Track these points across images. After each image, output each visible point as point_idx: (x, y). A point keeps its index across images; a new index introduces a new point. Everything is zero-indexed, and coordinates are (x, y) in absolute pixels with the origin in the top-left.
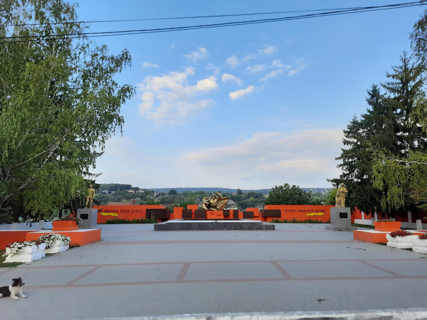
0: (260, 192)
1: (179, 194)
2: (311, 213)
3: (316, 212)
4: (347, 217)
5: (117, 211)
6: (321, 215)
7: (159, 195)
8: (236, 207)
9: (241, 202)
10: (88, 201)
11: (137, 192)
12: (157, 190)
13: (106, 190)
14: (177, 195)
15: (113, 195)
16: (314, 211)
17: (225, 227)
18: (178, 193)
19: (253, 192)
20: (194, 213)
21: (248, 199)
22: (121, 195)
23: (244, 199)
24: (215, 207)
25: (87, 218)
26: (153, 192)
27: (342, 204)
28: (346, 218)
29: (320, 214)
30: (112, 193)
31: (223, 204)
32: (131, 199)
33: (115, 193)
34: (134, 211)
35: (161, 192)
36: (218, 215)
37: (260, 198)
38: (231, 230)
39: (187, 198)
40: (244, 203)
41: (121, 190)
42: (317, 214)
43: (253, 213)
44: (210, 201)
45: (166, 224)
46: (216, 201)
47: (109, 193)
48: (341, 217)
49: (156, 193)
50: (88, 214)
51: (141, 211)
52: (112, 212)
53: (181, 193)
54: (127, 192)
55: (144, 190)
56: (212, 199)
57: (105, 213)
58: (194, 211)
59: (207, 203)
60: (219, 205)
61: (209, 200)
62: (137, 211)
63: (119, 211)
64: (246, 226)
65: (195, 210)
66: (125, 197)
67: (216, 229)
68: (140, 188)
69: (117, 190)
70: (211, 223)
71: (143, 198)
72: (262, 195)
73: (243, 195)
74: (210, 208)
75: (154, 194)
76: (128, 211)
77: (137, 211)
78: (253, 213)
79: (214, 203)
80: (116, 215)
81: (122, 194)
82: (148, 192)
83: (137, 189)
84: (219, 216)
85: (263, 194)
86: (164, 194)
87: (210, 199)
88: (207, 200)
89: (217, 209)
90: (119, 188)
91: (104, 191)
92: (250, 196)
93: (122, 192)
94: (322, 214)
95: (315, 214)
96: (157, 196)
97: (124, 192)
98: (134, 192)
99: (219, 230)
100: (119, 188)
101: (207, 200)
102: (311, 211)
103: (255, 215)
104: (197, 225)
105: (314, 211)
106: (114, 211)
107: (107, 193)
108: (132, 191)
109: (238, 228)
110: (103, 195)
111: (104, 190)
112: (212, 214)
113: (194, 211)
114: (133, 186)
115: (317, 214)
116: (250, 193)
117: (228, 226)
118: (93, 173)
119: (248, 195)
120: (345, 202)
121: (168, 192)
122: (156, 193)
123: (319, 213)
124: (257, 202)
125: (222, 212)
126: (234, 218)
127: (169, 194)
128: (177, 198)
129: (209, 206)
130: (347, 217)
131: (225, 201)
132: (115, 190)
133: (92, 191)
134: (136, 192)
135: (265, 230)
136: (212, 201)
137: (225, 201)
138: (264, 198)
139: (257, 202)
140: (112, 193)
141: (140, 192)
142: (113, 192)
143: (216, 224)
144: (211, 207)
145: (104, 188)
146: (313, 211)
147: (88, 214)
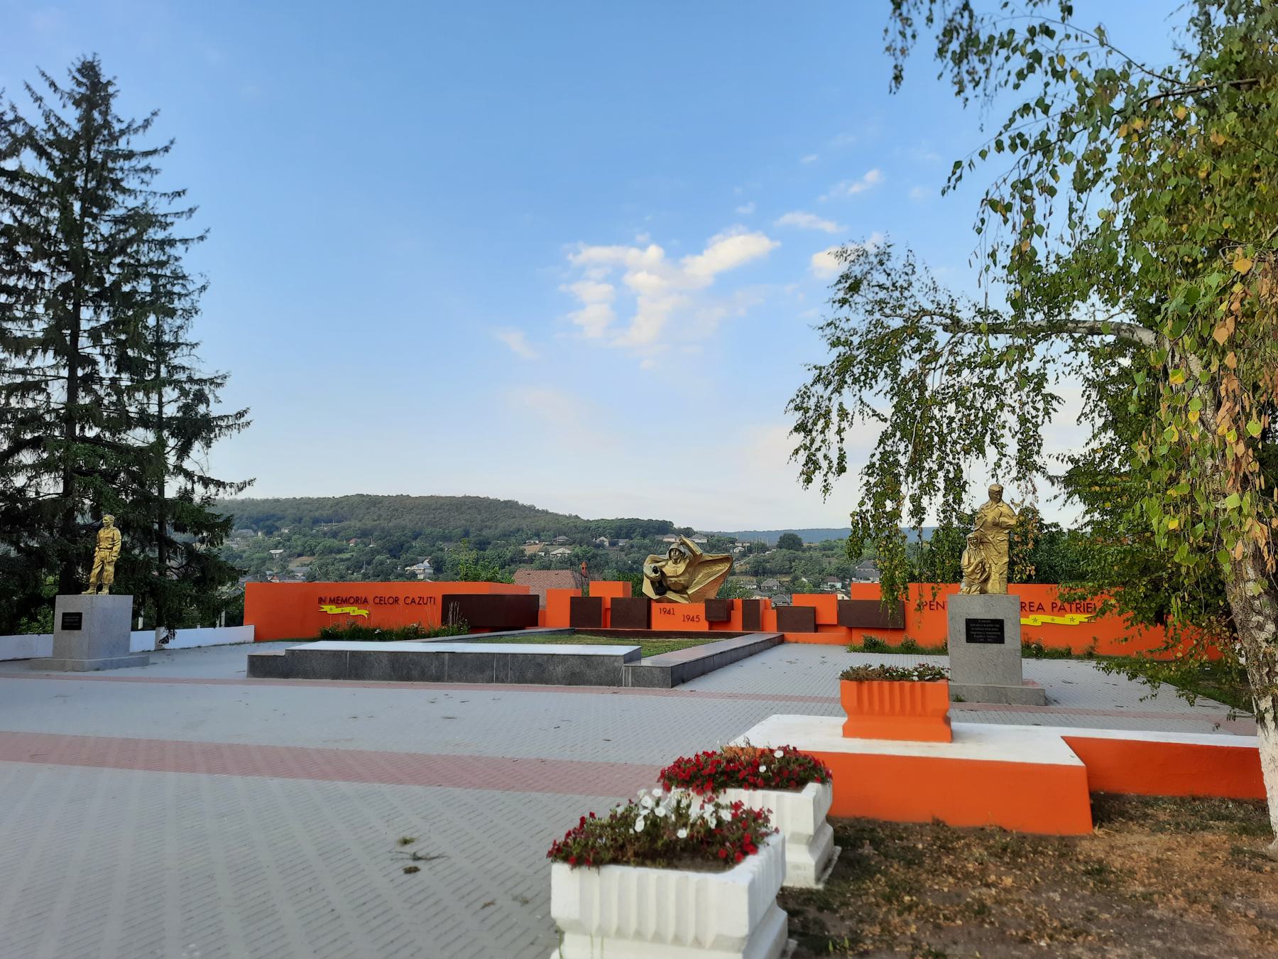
1: (810, 548)
2: (1032, 617)
3: (1055, 610)
4: (1000, 639)
5: (366, 601)
6: (1039, 623)
7: (750, 550)
10: (97, 571)
14: (804, 551)
15: (622, 549)
16: (1047, 607)
17: (483, 672)
18: (805, 545)
24: (682, 590)
25: (79, 628)
26: (733, 541)
27: (993, 577)
28: (995, 645)
29: (1072, 619)
30: (620, 544)
31: (712, 579)
34: (413, 601)
38: (503, 681)
39: (834, 560)
41: (644, 536)
42: (1058, 620)
44: (664, 570)
45: (283, 654)
46: (681, 567)
47: (613, 544)
48: (970, 638)
49: (740, 545)
50: (80, 615)
52: (352, 604)
53: (817, 544)
54: (661, 542)
55: (707, 535)
57: (333, 607)
60: (698, 583)
62: (421, 602)
63: (370, 600)
64: (560, 670)
65: (612, 599)
67: (451, 679)
69: (633, 536)
70: (434, 653)
74: (665, 593)
76: (396, 600)
77: (421, 602)
79: (677, 577)
80: (364, 612)
82: (718, 541)
83: (688, 532)
84: (693, 620)
86: (764, 548)
87: (664, 560)
89: (690, 598)
91: (598, 541)
93: (647, 541)
94: (1079, 618)
95: (1047, 618)
96: (744, 555)
97: (652, 541)
99: (460, 680)
102: (1035, 609)
104: (385, 661)
105: (1047, 607)
106: (357, 601)
107: (607, 544)
109: (529, 675)
111: (600, 536)
114: (676, 526)
115: (1058, 620)
118: (227, 481)
120: (1006, 566)
121: (776, 541)
122: (740, 545)
123: (1069, 616)
126: (743, 629)
127: (780, 547)
128: (801, 559)
129: (661, 585)
130: (1000, 639)
132: (628, 536)
133: (111, 535)
135: (633, 685)
137: (718, 568)
142: (622, 543)
143: (450, 659)
144: (670, 589)
146: (1041, 609)
147: (81, 614)
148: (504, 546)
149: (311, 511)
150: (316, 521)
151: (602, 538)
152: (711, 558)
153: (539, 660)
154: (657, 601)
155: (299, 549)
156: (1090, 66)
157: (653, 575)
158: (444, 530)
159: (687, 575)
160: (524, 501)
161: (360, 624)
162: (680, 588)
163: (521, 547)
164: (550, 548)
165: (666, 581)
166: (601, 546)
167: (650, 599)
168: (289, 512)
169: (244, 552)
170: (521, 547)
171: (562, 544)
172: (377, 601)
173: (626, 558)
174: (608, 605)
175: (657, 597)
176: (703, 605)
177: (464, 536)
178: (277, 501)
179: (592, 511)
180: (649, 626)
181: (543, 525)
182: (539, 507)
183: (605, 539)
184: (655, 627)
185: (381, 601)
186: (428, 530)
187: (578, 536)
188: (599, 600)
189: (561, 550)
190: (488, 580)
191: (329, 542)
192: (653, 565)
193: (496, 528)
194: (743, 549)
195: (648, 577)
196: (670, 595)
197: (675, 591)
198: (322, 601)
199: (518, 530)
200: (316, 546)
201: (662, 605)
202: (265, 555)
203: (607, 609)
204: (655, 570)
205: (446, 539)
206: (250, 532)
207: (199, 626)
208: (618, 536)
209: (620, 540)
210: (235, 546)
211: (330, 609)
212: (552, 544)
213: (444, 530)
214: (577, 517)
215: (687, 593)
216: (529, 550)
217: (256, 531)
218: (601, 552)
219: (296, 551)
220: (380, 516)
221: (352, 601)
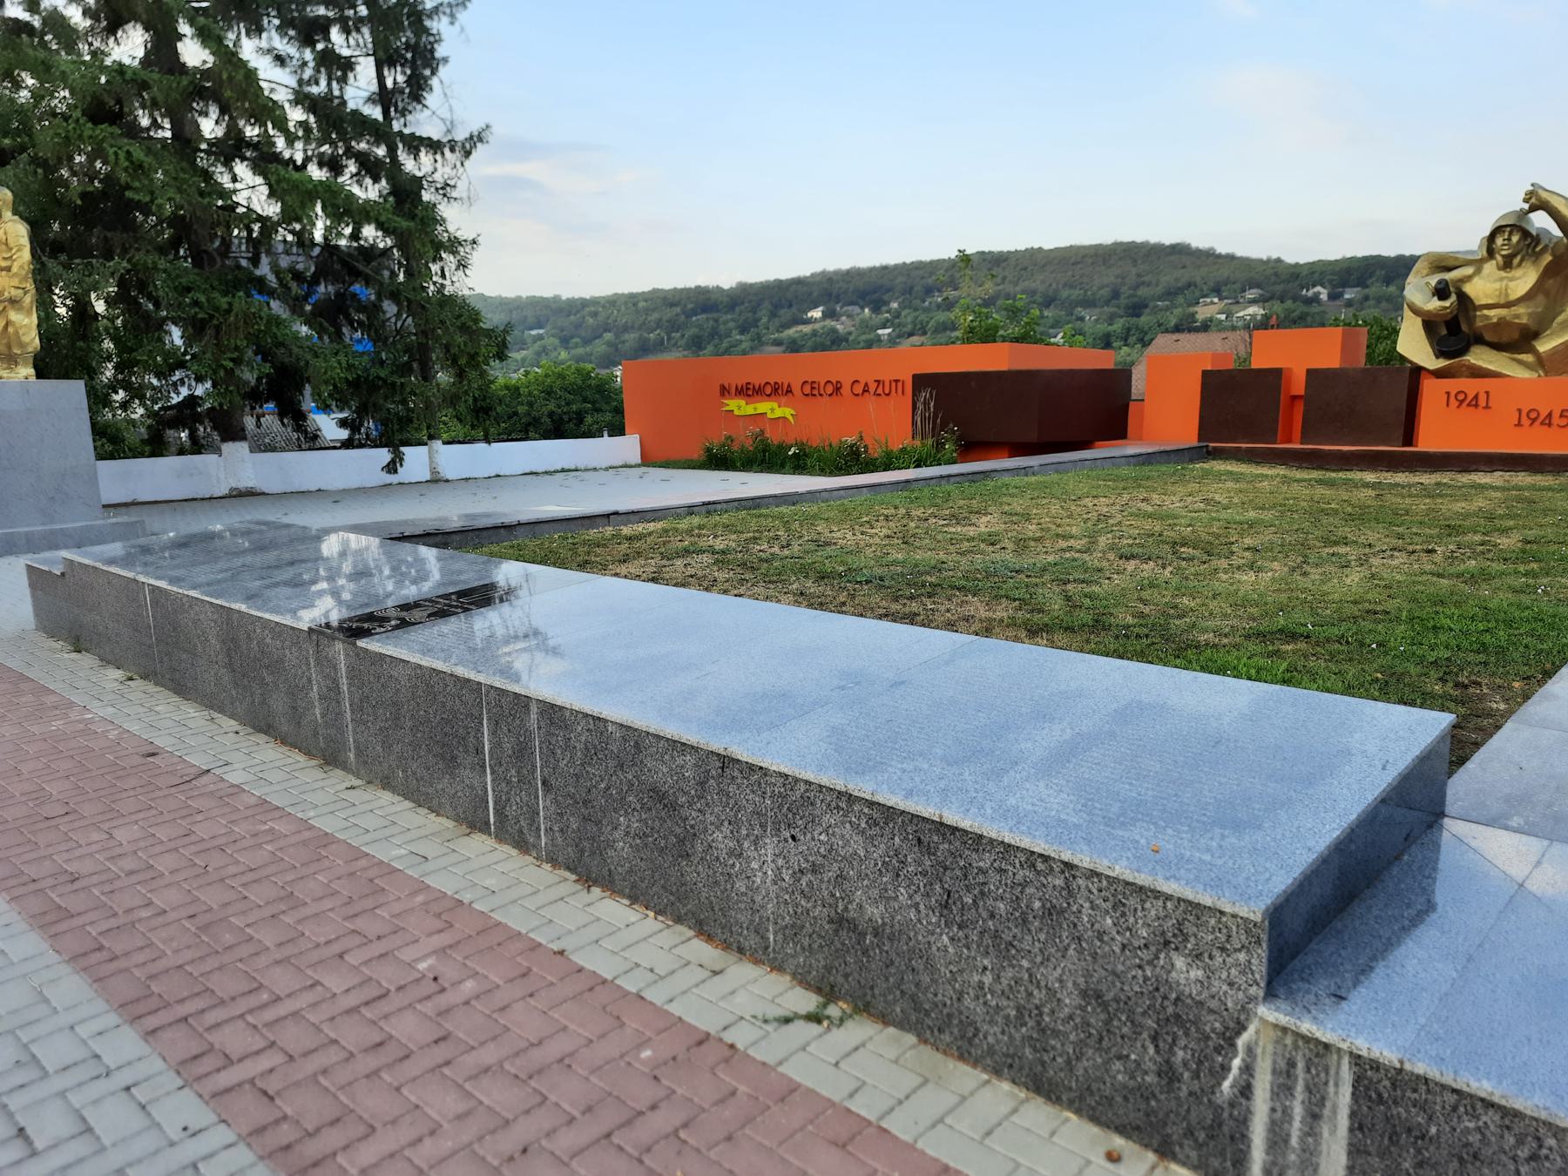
5: (789, 391)
13: (1323, 286)
15: (1349, 304)
22: (1384, 305)
24: (1518, 340)
33: (1359, 297)
34: (866, 390)
44: (1468, 289)
46: (1525, 279)
47: (1332, 297)
51: (900, 384)
56: (1490, 267)
62: (880, 391)
63: (796, 389)
65: (1311, 373)
69: (1369, 282)
74: (1464, 351)
77: (880, 391)
79: (1508, 305)
80: (787, 412)
89: (1542, 362)
90: (1380, 273)
91: (1310, 293)
100: (1378, 273)
106: (777, 391)
107: (1324, 297)
110: (1301, 308)
111: (1314, 286)
112: (1475, 402)
117: (479, 751)
132: (1361, 283)
142: (1349, 295)
144: (1479, 340)
148: (1167, 309)
149: (922, 278)
150: (929, 291)
151: (1318, 289)
153: (660, 772)
155: (910, 327)
156: (721, 972)
157: (1434, 304)
158: (1086, 291)
159: (1541, 299)
160: (1198, 242)
161: (774, 437)
163: (1192, 310)
164: (1234, 308)
165: (1471, 321)
166: (1315, 299)
167: (1417, 371)
168: (898, 281)
169: (850, 333)
170: (1192, 310)
171: (1253, 302)
172: (807, 389)
174: (1299, 386)
175: (1442, 363)
177: (1113, 298)
178: (885, 268)
179: (1299, 251)
180: (1409, 439)
181: (1226, 275)
182: (1222, 249)
184: (1427, 442)
185: (813, 390)
186: (1065, 294)
187: (1279, 288)
189: (1252, 310)
191: (942, 316)
192: (1433, 281)
193: (1157, 285)
195: (1416, 311)
196: (1479, 357)
197: (1497, 347)
198: (724, 391)
199: (1189, 285)
200: (928, 323)
201: (1453, 385)
202: (872, 336)
203: (1294, 398)
204: (1441, 292)
205: (1088, 303)
206: (856, 309)
207: (606, 434)
208: (1345, 284)
209: (1347, 290)
210: (839, 327)
211: (739, 406)
212: (1238, 303)
213: (1086, 291)
214: (1279, 260)
215: (1533, 351)
216: (1203, 312)
217: (862, 308)
219: (905, 329)
220: (1004, 278)
221: (768, 390)
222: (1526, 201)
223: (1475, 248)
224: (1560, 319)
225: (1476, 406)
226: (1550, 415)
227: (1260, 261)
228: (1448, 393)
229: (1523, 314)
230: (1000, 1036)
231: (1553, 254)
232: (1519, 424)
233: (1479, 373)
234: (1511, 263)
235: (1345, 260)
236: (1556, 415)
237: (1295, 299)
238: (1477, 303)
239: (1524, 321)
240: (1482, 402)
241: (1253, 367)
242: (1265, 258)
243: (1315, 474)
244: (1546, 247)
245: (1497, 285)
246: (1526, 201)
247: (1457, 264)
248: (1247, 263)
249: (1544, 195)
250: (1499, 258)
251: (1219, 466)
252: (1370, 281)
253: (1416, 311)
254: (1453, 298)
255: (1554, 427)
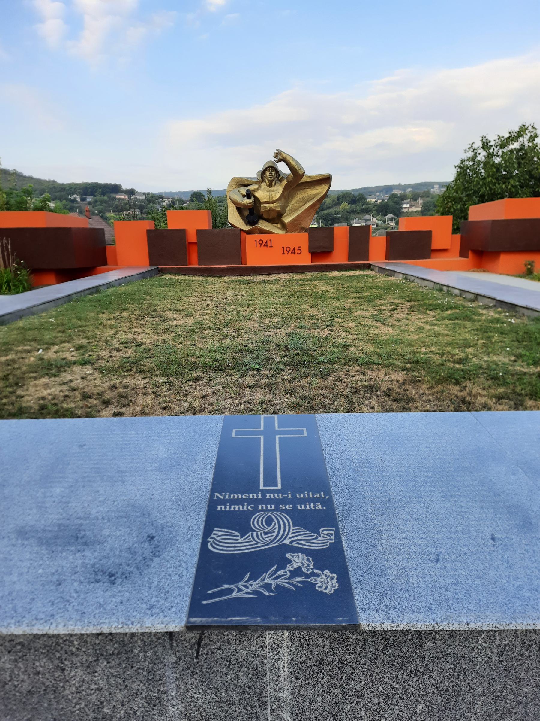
0: (361, 192)
8: (315, 223)
9: (325, 212)
11: (133, 197)
12: (170, 195)
13: (76, 194)
15: (90, 203)
19: (347, 193)
20: (195, 243)
21: (337, 207)
22: (104, 204)
23: (330, 208)
26: (161, 197)
30: (88, 200)
32: (123, 211)
33: (93, 200)
35: (176, 197)
36: (289, 251)
37: (361, 204)
40: (329, 214)
41: (103, 194)
43: (428, 235)
44: (257, 194)
46: (278, 190)
47: (83, 200)
49: (166, 200)
54: (115, 199)
55: (144, 194)
56: (263, 185)
58: (192, 237)
59: (246, 201)
60: (293, 211)
61: (251, 188)
66: (111, 208)
68: (137, 190)
71: (145, 210)
72: (363, 198)
73: (328, 199)
74: (255, 223)
75: (163, 202)
78: (428, 235)
79: (273, 202)
81: (105, 202)
82: (153, 197)
83: (131, 192)
85: (367, 197)
88: (244, 191)
89: (284, 226)
91: (73, 197)
92: (341, 200)
93: (106, 198)
97: (109, 197)
98: (126, 197)
100: (99, 190)
101: (244, 191)
103: (434, 246)
108: (122, 197)
111: (73, 194)
113: (192, 237)
114: (124, 187)
116: (341, 194)
119: (338, 199)
121: (188, 198)
124: (353, 212)
125: (307, 234)
127: (191, 200)
131: (317, 191)
132: (92, 194)
134: (130, 199)
136: (262, 194)
138: (368, 203)
139: (353, 212)
140: (88, 200)
141: (138, 197)
142: (89, 199)
144: (261, 217)
145: (73, 190)
151: (75, 196)
152: (309, 180)
154: (249, 232)
159: (283, 199)
162: (273, 215)
166: (74, 201)
173: (93, 209)
176: (305, 236)
183: (77, 197)
188: (182, 232)
190: (37, 209)
194: (168, 203)
197: (268, 220)
209: (88, 197)
214: (54, 181)
218: (76, 205)
222: (275, 157)
223: (256, 176)
224: (289, 208)
225: (267, 246)
226: (294, 249)
227: (45, 181)
228: (256, 241)
229: (277, 206)
230: (484, 644)
231: (288, 181)
232: (283, 254)
233: (263, 232)
234: (272, 184)
235: (84, 184)
236: (296, 249)
237: (67, 200)
238: (261, 201)
239: (279, 209)
240: (269, 244)
241: (170, 227)
242: (47, 180)
243: (241, 278)
244: (283, 177)
245: (268, 194)
246: (275, 157)
247: (249, 183)
248: (39, 182)
249: (284, 155)
250: (267, 181)
251: (167, 276)
252: (96, 193)
253: (234, 202)
254: (253, 198)
255: (296, 254)
